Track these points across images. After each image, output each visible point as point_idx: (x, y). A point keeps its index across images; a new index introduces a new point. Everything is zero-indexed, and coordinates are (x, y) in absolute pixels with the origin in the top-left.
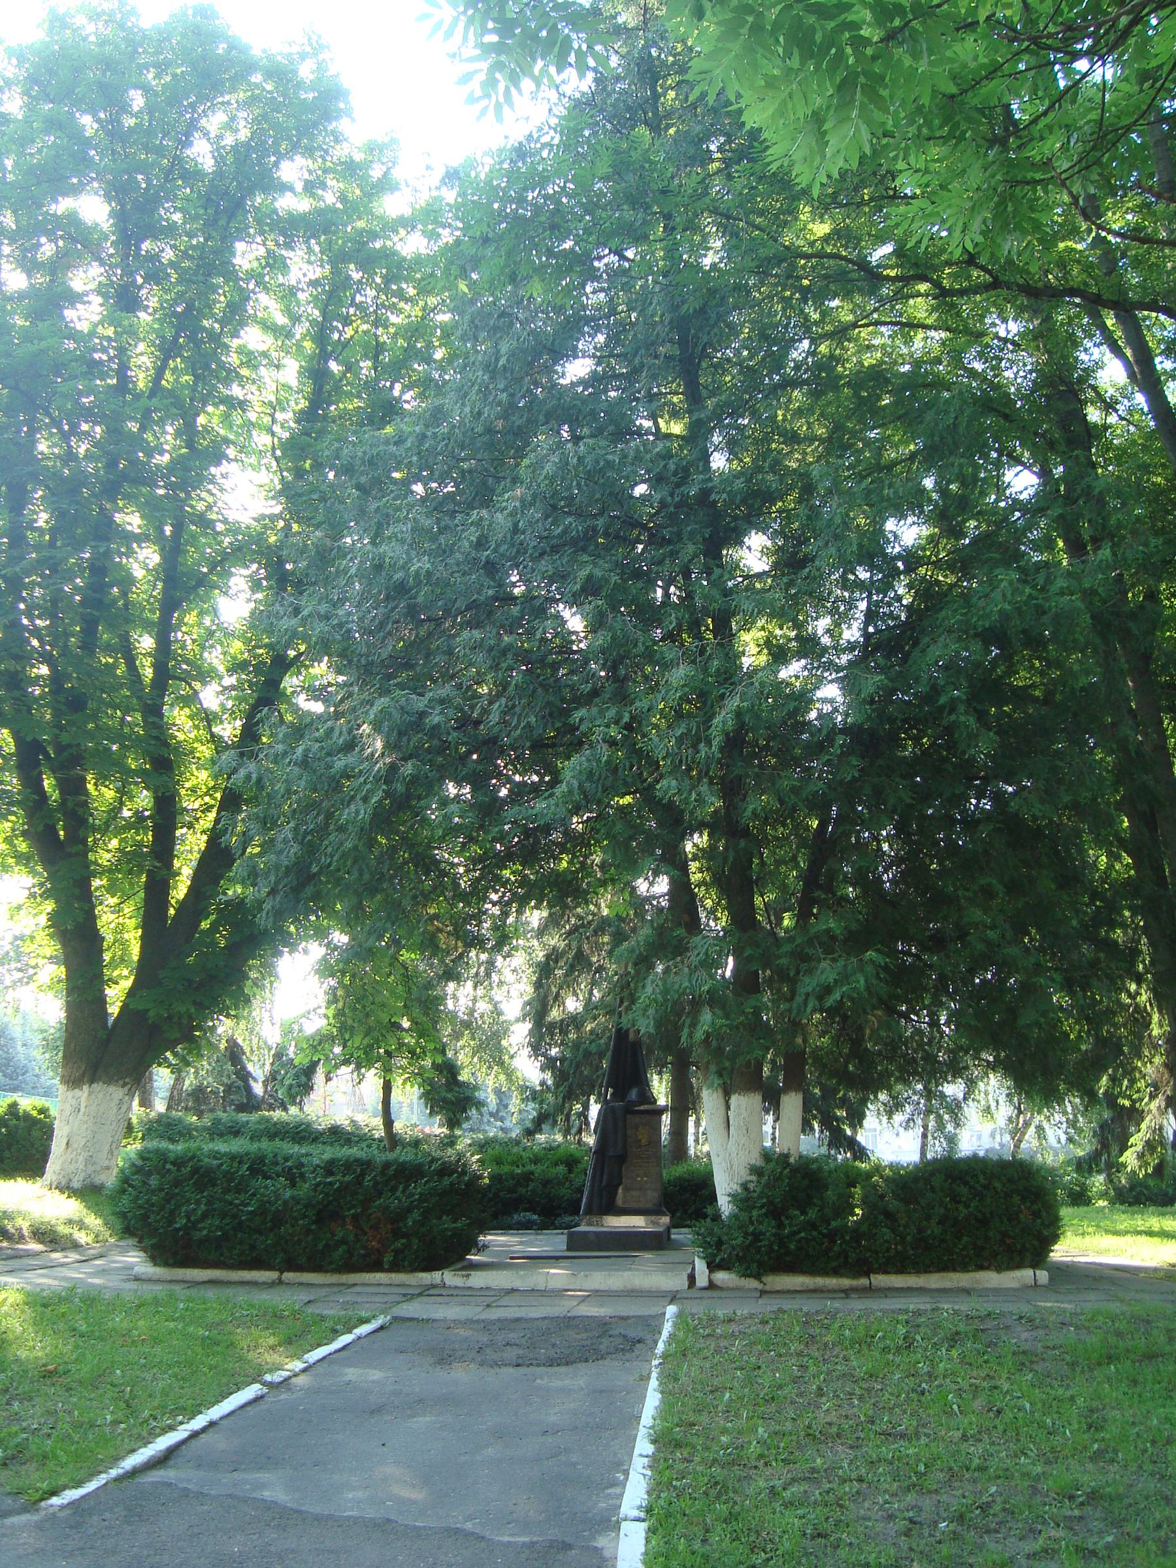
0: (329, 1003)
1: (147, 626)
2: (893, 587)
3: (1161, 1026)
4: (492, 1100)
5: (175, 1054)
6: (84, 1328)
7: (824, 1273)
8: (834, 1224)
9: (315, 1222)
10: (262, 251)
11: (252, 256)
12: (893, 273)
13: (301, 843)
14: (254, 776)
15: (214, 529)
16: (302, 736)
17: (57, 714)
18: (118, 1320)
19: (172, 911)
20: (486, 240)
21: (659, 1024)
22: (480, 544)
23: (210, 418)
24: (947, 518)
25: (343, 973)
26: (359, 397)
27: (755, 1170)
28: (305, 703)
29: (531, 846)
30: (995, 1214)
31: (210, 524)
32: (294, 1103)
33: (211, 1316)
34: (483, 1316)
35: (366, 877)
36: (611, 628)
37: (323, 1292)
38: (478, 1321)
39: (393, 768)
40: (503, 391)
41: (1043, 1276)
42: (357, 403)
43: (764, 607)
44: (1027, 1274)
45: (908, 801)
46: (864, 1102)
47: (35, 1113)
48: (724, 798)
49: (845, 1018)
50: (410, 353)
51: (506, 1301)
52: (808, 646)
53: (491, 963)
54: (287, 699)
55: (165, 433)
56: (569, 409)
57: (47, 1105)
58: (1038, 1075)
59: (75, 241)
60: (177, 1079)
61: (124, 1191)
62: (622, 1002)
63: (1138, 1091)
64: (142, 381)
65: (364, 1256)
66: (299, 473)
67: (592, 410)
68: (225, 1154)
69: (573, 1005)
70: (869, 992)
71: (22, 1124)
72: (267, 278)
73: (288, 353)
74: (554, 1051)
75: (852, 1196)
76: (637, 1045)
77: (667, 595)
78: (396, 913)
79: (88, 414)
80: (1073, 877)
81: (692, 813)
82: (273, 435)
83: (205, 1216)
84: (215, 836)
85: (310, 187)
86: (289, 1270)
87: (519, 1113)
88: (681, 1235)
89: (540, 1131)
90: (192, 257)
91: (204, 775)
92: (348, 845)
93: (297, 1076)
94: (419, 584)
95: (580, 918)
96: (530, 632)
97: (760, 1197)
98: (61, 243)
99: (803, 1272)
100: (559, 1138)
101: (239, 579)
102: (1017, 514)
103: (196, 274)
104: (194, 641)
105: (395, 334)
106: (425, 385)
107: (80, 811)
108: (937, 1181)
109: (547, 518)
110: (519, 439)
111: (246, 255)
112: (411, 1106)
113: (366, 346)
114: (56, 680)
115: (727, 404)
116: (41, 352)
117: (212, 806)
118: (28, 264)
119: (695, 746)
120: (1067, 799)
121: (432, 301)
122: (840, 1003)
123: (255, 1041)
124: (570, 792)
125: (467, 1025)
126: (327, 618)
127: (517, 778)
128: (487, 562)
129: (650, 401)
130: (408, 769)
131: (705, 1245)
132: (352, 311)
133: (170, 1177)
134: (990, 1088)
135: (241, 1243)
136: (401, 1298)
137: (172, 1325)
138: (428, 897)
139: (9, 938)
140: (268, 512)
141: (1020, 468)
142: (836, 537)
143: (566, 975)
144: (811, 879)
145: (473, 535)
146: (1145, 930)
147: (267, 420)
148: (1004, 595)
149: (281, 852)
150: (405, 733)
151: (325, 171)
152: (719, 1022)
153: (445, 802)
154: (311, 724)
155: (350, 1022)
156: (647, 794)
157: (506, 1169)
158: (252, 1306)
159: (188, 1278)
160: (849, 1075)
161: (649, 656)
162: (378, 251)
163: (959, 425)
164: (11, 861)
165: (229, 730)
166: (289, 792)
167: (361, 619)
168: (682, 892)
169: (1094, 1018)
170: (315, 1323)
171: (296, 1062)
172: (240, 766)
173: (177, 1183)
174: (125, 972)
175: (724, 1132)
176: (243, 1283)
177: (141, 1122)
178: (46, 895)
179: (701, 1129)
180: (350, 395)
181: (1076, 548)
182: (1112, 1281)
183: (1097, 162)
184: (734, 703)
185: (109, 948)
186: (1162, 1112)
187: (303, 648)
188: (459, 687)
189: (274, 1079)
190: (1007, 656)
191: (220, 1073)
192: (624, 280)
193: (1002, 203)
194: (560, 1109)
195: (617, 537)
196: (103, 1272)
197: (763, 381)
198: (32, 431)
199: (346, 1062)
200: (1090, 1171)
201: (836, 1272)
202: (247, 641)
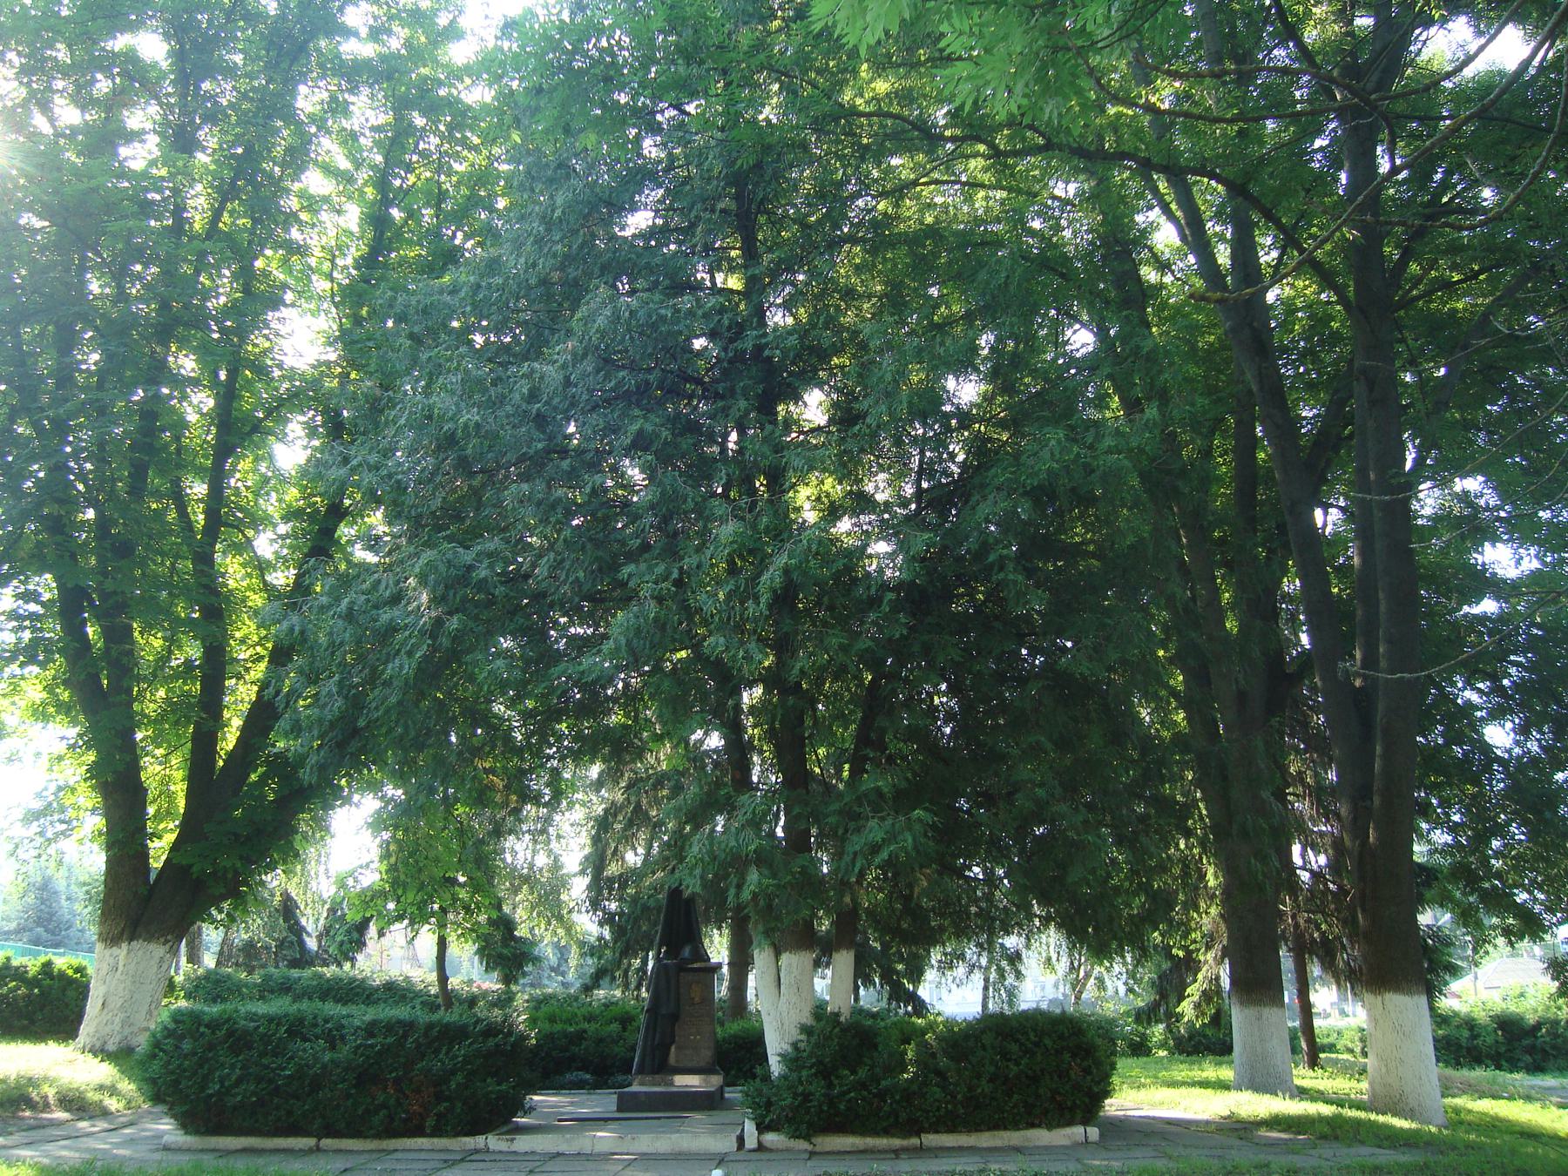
1: (200, 471)
3: (1216, 877)
7: (875, 1133)
9: (355, 1086)
10: (325, 95)
11: (316, 99)
13: (346, 697)
20: (539, 91)
22: (533, 396)
23: (268, 261)
24: (1002, 375)
25: (396, 827)
26: (421, 245)
27: (806, 1030)
28: (361, 554)
30: (1050, 1069)
32: (347, 958)
37: (362, 1159)
39: (438, 623)
41: (1094, 1132)
44: (1077, 1131)
47: (70, 972)
50: (473, 202)
52: (861, 502)
54: (342, 549)
55: (220, 276)
57: (84, 963)
58: (1094, 931)
61: (154, 1056)
63: (1195, 942)
64: (199, 223)
65: (405, 1121)
66: (357, 321)
68: (263, 1016)
69: (633, 858)
70: (918, 852)
72: (330, 123)
74: (613, 906)
78: (445, 770)
79: (139, 254)
80: (1121, 728)
85: (376, 34)
87: (576, 969)
88: (733, 1094)
90: (252, 99)
92: (393, 700)
93: (349, 932)
97: (810, 1056)
98: (118, 80)
99: (853, 1132)
100: (618, 993)
101: (296, 427)
103: (255, 116)
105: (459, 182)
106: (488, 234)
107: (125, 660)
108: (987, 1039)
109: (598, 372)
110: (575, 292)
111: (308, 99)
112: (471, 960)
113: (429, 193)
114: (102, 524)
116: (94, 190)
117: (263, 657)
118: (82, 100)
121: (496, 151)
124: (618, 649)
125: (526, 879)
128: (538, 415)
130: (454, 623)
131: (755, 1106)
132: (415, 158)
134: (1052, 940)
135: (277, 1108)
140: (324, 358)
141: (1077, 326)
143: (624, 830)
144: (862, 739)
146: (1197, 783)
147: (326, 266)
149: (325, 705)
150: (453, 588)
151: (391, 18)
152: (765, 881)
155: (402, 877)
157: (558, 1027)
159: (221, 1146)
162: (442, 98)
163: (1013, 282)
168: (738, 750)
173: (211, 1047)
174: (171, 826)
175: (774, 990)
176: (284, 1151)
178: (88, 746)
180: (410, 243)
183: (1138, 31)
185: (155, 800)
186: (1220, 962)
191: (273, 929)
193: (1044, 68)
196: (131, 1141)
198: (82, 269)
199: (400, 918)
201: (886, 1132)
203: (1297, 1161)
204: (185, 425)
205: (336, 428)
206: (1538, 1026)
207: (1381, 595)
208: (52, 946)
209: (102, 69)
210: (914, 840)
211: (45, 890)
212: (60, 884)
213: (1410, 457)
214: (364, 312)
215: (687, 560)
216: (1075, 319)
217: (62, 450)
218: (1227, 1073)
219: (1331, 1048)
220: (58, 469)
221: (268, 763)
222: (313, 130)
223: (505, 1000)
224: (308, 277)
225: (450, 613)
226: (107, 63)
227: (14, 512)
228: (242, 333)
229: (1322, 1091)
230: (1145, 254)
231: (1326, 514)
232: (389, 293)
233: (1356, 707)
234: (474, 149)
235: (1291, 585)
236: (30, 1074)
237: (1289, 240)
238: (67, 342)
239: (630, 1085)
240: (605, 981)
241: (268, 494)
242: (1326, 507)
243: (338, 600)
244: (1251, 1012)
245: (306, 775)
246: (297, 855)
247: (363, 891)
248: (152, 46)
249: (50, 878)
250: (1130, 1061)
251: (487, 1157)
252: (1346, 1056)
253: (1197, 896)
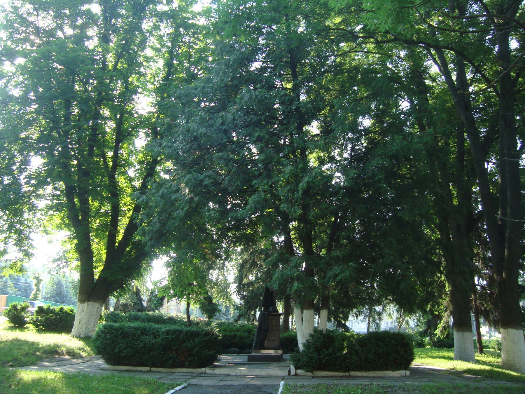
0: (169, 276)
1: (110, 148)
2: (360, 140)
3: (449, 288)
4: (224, 309)
5: (117, 292)
6: (83, 386)
7: (334, 371)
8: (338, 354)
12: (361, 35)
13: (160, 223)
14: (145, 200)
15: (133, 116)
16: (161, 187)
17: (79, 177)
18: (94, 384)
19: (117, 244)
20: (226, 22)
21: (280, 286)
22: (223, 124)
23: (133, 79)
24: (379, 118)
25: (174, 266)
29: (239, 225)
30: (392, 351)
31: (133, 115)
32: (157, 309)
33: (126, 383)
34: (218, 384)
35: (182, 235)
36: (266, 153)
37: (165, 375)
38: (217, 386)
39: (192, 198)
40: (231, 72)
41: (408, 373)
42: (182, 75)
43: (317, 146)
44: (402, 372)
45: (364, 212)
46: (348, 313)
47: (69, 311)
48: (303, 210)
49: (342, 285)
51: (226, 379)
52: (332, 159)
53: (224, 264)
54: (157, 174)
55: (118, 84)
56: (253, 78)
57: (73, 308)
58: (407, 306)
59: (89, 19)
60: (117, 300)
61: (98, 339)
62: (267, 278)
66: (163, 98)
67: (261, 80)
68: (133, 327)
69: (251, 278)
70: (351, 277)
71: (65, 315)
73: (160, 57)
74: (245, 293)
75: (343, 344)
76: (272, 293)
77: (285, 142)
78: (192, 247)
79: (92, 77)
80: (419, 237)
81: (292, 216)
82: (154, 85)
83: (125, 348)
84: (132, 220)
86: (153, 367)
88: (287, 356)
89: (240, 320)
91: (128, 199)
92: (176, 224)
93: (158, 300)
94: (201, 137)
95: (254, 249)
96: (239, 154)
97: (312, 345)
98: (84, 20)
100: (246, 322)
101: (142, 133)
102: (403, 116)
103: (129, 31)
104: (126, 153)
106: (206, 69)
110: (236, 89)
111: (146, 25)
113: (186, 56)
114: (79, 165)
115: (305, 78)
116: (77, 56)
117: (131, 209)
118: (73, 26)
119: (293, 193)
120: (417, 212)
122: (341, 279)
123: (145, 288)
124: (251, 208)
125: (216, 284)
126: (170, 147)
127: (234, 202)
129: (280, 77)
130: (197, 199)
131: (294, 361)
132: (181, 44)
134: (391, 308)
136: (190, 377)
137: (113, 386)
138: (203, 242)
139: (62, 251)
140: (152, 111)
141: (403, 100)
142: (341, 123)
143: (249, 268)
145: (220, 121)
146: (443, 255)
147: (152, 81)
148: (397, 144)
149: (154, 226)
150: (196, 187)
153: (209, 210)
154: (165, 183)
156: (277, 208)
157: (228, 333)
158: (140, 379)
159: (119, 369)
160: (341, 307)
161: (279, 163)
164: (63, 226)
165: (137, 184)
166: (157, 206)
167: (182, 148)
169: (424, 284)
170: (161, 386)
171: (158, 296)
172: (141, 197)
173: (116, 337)
174: (101, 264)
175: (301, 323)
177: (105, 314)
178: (74, 238)
179: (294, 320)
180: (180, 72)
181: (422, 128)
182: (431, 374)
184: (306, 179)
186: (449, 316)
187: (163, 157)
188: (214, 172)
189: (150, 301)
190: (398, 164)
191: (132, 299)
192: (272, 36)
194: (246, 313)
195: (268, 122)
196: (90, 366)
197: (316, 73)
198: (73, 82)
199: (175, 296)
200: (424, 336)
201: (338, 370)
202: (144, 154)
203: (479, 385)
204: (106, 133)
205: (155, 133)
207: (508, 192)
208: (61, 303)
209: (80, 16)
210: (350, 273)
211: (59, 284)
212: (64, 283)
213: (519, 145)
214: (165, 95)
215: (274, 179)
216: (403, 98)
217: (67, 141)
218: (452, 355)
219: (487, 347)
220: (65, 147)
221: (132, 244)
222: (148, 34)
223: (208, 324)
224: (146, 84)
225: (196, 196)
226: (82, 14)
227: (52, 161)
228: (125, 101)
229: (483, 362)
230: (427, 75)
231: (488, 164)
232: (175, 89)
233: (498, 231)
234: (200, 41)
235: (476, 189)
236: (57, 343)
237: (477, 70)
238: (68, 106)
239: (251, 353)
240: (241, 319)
241: (132, 156)
242: (488, 162)
243: (158, 191)
244: (460, 334)
245: (147, 249)
246: (142, 275)
247: (163, 287)
248: (96, 9)
249: (61, 280)
250: (418, 349)
251: (206, 375)
252: (492, 350)
253: (442, 294)
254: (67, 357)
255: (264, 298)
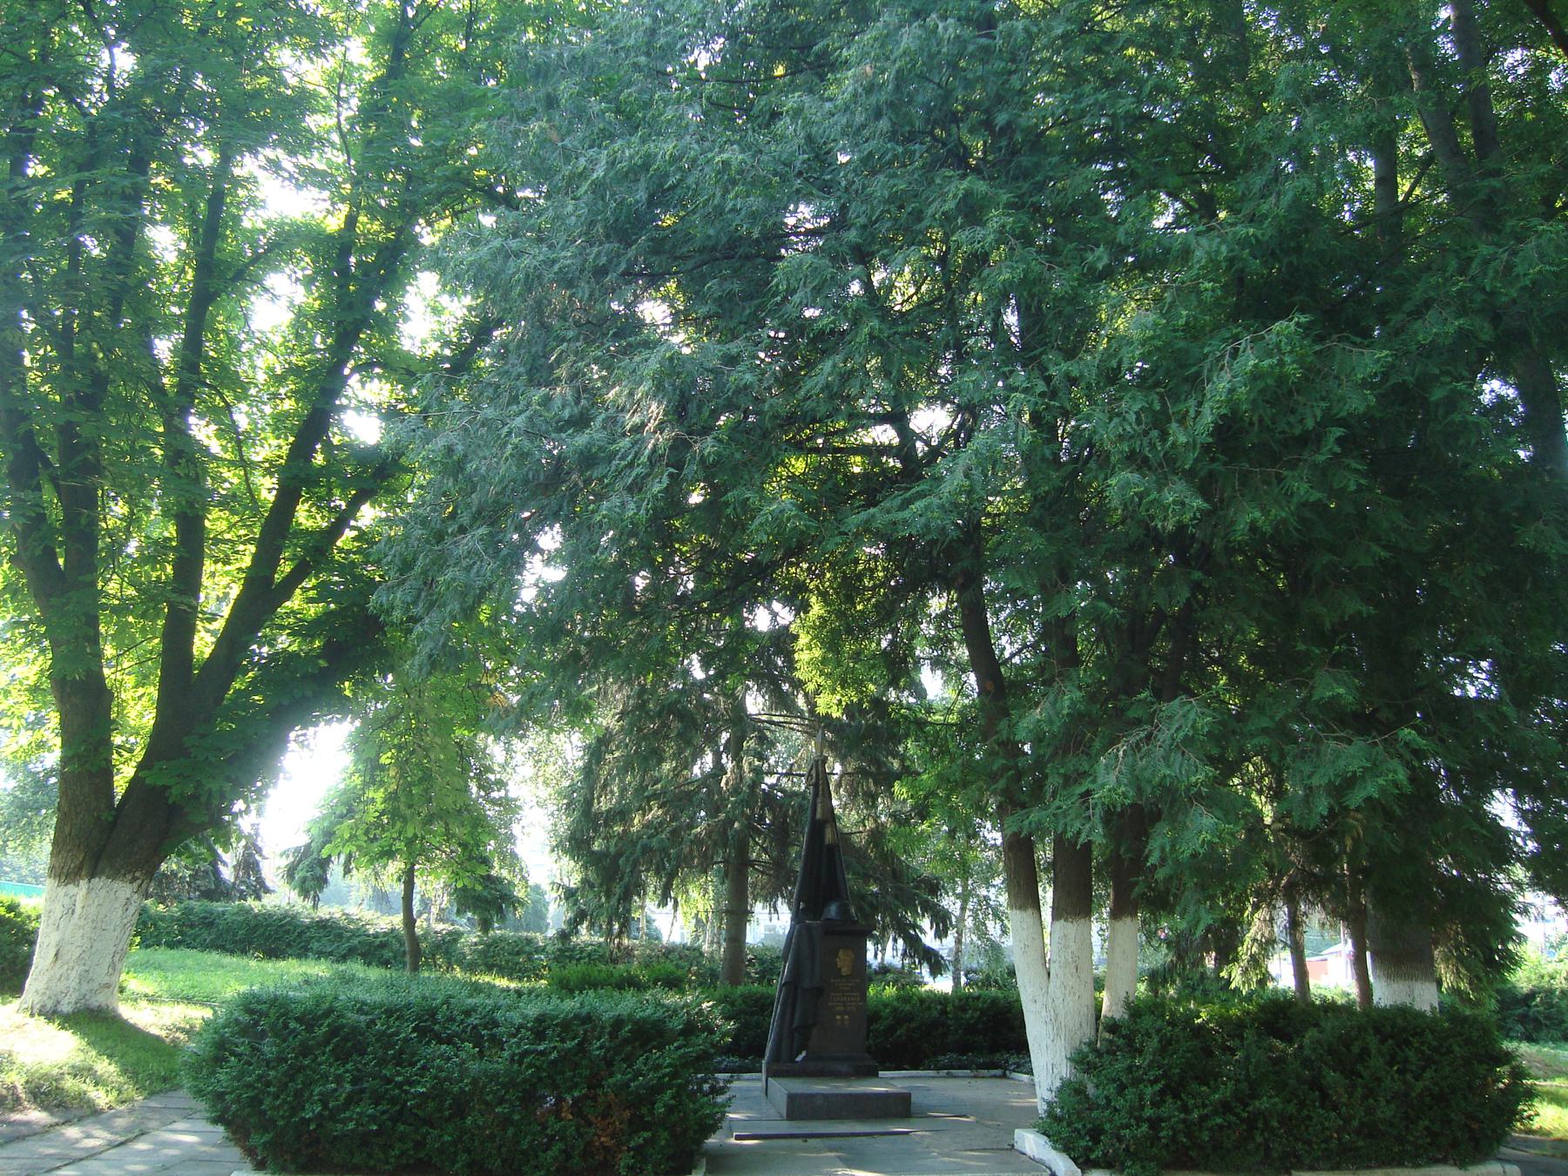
68: (374, 1007)
83: (351, 1100)
133: (294, 1043)
135: (402, 1139)
173: (305, 1051)
206: (1532, 995)
254: (36, 1115)
255: (805, 868)
